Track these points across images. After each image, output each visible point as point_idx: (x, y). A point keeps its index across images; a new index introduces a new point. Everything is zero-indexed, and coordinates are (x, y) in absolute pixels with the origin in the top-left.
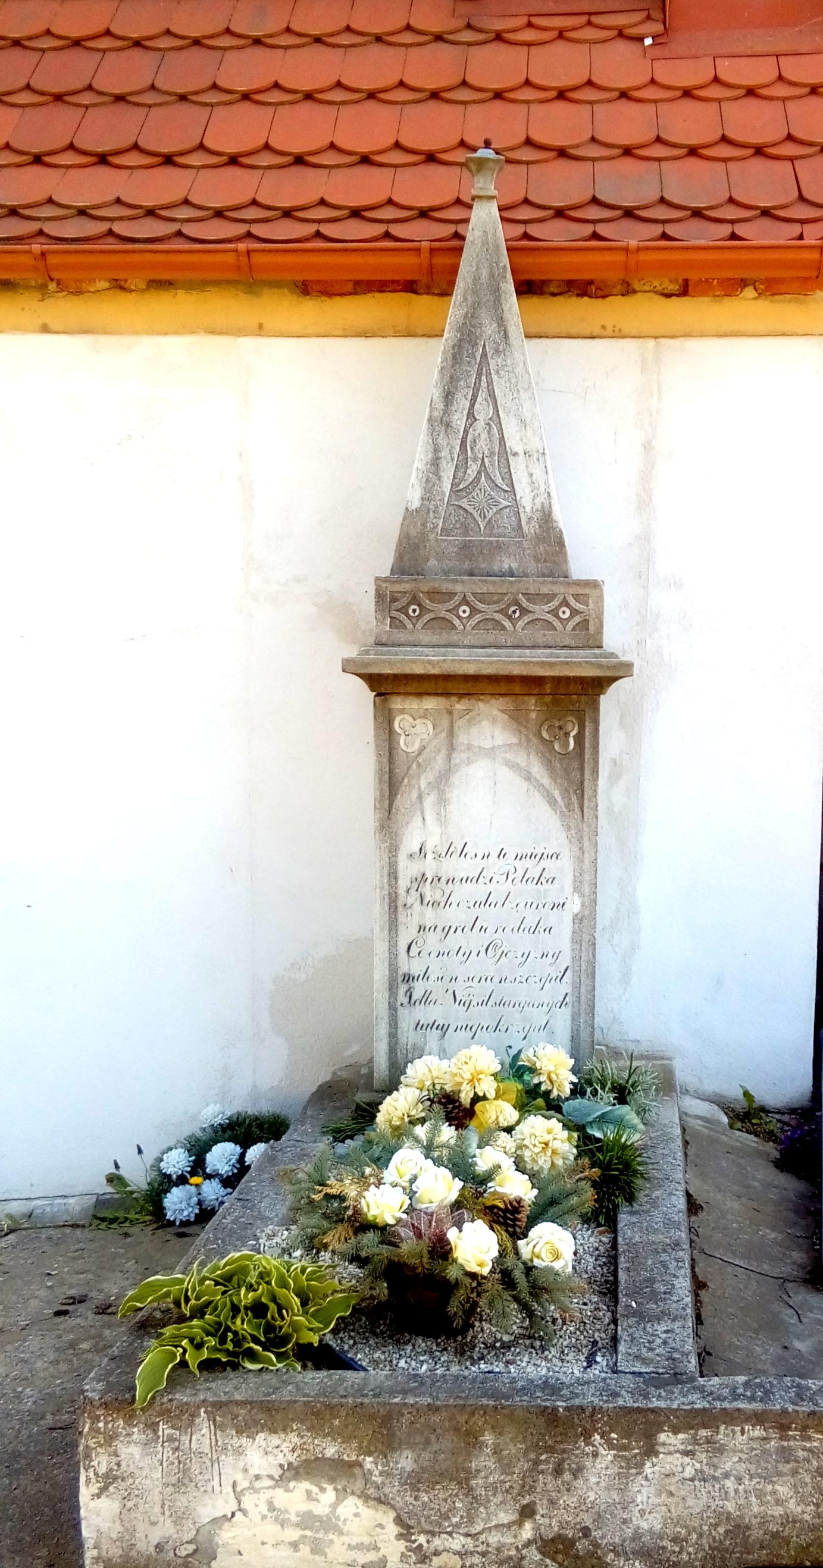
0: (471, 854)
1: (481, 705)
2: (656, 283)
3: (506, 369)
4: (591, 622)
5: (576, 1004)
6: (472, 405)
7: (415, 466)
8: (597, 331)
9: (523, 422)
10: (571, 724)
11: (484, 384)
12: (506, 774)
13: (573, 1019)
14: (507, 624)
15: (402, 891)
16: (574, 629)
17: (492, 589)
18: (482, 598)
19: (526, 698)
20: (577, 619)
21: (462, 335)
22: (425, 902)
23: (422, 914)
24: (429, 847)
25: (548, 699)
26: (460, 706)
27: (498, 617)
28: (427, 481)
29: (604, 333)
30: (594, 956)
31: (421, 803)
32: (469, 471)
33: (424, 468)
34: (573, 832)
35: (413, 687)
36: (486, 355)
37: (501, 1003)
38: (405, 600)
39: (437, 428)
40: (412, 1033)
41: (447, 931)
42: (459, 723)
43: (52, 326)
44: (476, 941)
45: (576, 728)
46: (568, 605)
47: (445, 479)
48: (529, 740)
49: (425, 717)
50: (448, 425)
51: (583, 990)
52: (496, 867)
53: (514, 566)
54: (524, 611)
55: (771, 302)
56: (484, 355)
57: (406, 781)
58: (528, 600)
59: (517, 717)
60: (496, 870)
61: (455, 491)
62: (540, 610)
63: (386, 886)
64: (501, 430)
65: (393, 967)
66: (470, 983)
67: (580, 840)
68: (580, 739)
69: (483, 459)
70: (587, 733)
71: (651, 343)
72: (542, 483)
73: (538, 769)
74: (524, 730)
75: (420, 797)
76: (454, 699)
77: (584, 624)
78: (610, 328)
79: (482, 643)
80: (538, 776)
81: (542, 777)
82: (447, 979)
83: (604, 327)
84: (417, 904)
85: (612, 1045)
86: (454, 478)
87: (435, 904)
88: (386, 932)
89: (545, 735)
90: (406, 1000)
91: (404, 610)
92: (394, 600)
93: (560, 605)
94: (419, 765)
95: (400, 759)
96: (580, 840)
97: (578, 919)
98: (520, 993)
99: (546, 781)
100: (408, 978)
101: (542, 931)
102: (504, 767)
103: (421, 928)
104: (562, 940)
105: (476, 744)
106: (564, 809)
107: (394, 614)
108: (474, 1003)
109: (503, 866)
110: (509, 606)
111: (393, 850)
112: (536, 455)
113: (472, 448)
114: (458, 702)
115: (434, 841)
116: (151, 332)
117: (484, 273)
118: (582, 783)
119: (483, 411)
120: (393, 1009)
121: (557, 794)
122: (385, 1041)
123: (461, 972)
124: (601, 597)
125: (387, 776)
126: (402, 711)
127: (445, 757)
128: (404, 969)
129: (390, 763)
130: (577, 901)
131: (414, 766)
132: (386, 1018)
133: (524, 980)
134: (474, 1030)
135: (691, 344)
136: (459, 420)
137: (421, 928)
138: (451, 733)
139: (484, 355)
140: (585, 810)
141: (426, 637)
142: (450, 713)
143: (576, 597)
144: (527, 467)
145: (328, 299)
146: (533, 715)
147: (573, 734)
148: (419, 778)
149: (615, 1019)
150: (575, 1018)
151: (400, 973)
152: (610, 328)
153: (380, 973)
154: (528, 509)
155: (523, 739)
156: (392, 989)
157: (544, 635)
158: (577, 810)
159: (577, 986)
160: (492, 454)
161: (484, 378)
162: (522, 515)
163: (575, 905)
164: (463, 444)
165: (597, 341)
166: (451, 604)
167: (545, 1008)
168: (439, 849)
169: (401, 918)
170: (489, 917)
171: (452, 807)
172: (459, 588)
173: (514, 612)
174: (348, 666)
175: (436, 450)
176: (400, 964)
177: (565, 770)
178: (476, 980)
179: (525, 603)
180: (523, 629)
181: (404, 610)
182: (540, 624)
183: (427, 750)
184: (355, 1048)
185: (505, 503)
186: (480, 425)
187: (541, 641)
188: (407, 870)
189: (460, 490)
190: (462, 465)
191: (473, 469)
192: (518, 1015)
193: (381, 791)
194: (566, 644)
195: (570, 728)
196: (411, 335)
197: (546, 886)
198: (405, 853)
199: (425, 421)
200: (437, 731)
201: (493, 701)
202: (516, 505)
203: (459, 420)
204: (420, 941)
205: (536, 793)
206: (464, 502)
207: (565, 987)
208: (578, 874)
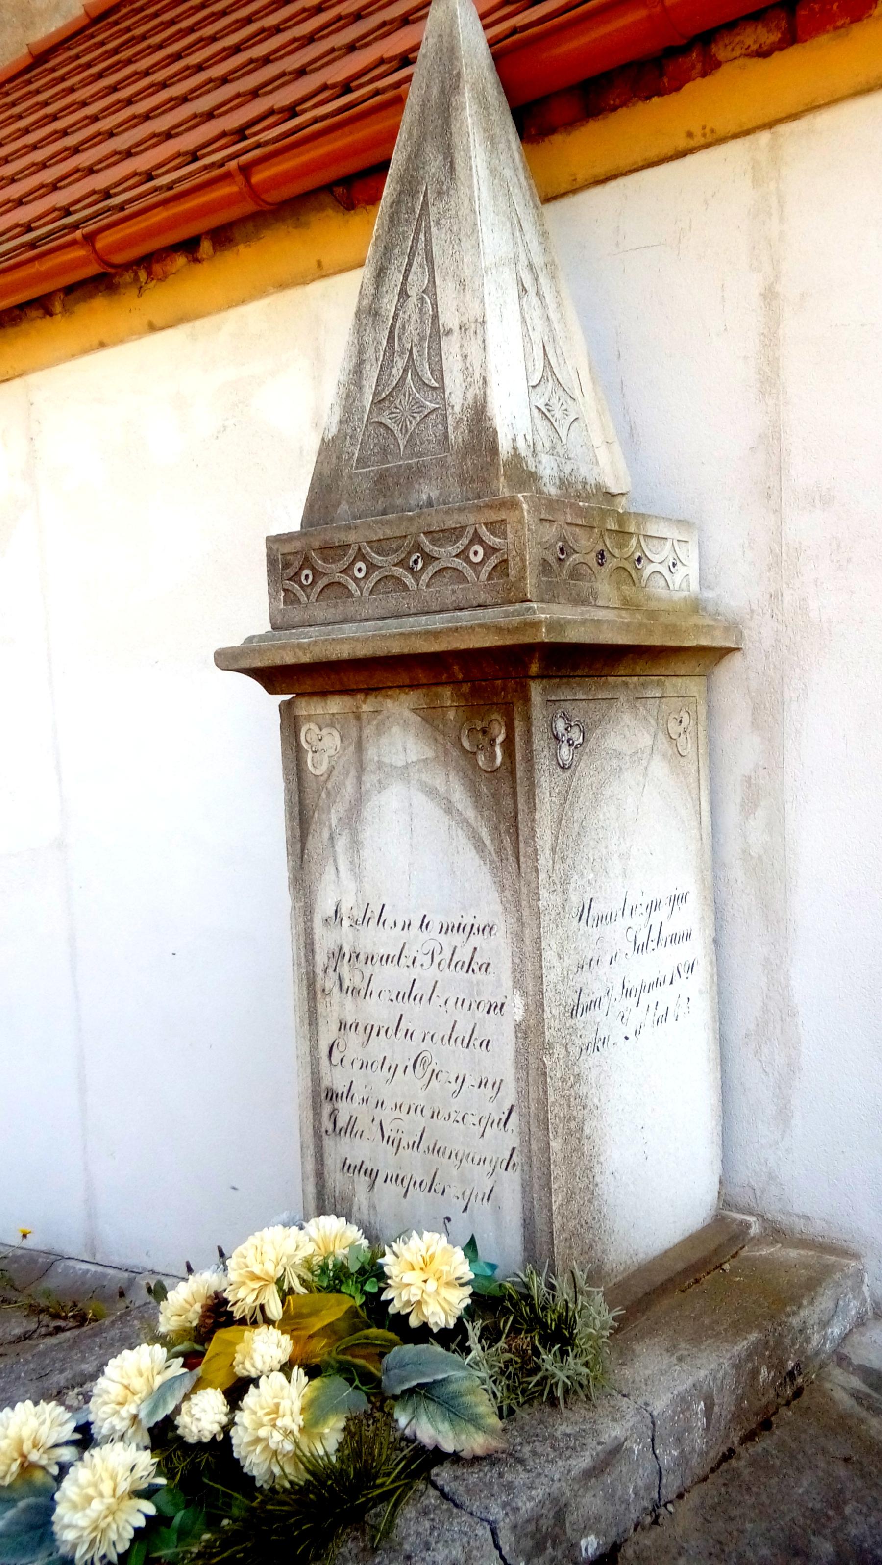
1: (389, 703)
2: (749, 41)
4: (511, 563)
5: (526, 1168)
6: (406, 277)
8: (682, 143)
9: (462, 284)
11: (421, 245)
12: (427, 810)
13: (524, 1192)
14: (409, 580)
15: (319, 970)
16: (490, 577)
17: (389, 533)
18: (380, 546)
19: (440, 689)
21: (403, 185)
22: (345, 987)
23: (342, 1005)
24: (344, 911)
28: (348, 396)
29: (692, 143)
31: (333, 847)
33: (346, 379)
36: (427, 204)
37: (435, 1150)
38: (297, 564)
41: (369, 1030)
42: (368, 731)
43: (158, 321)
44: (400, 1051)
45: (503, 731)
49: (332, 725)
50: (376, 314)
51: (534, 1147)
52: (420, 942)
53: (434, 494)
54: (429, 559)
56: (425, 203)
57: (316, 815)
58: (433, 542)
59: (430, 717)
60: (419, 947)
61: (378, 403)
62: (446, 554)
63: (303, 964)
64: (435, 306)
67: (518, 904)
68: (509, 745)
69: (411, 351)
70: (517, 739)
71: (764, 137)
72: (477, 365)
73: (459, 796)
74: (440, 738)
75: (331, 838)
76: (361, 696)
78: (698, 132)
81: (466, 808)
82: (372, 1102)
83: (690, 135)
84: (336, 989)
85: (769, 1216)
86: (377, 385)
87: (355, 991)
88: (307, 1027)
89: (466, 744)
90: (330, 1127)
91: (295, 577)
92: (286, 565)
94: (329, 794)
95: (311, 785)
96: (518, 904)
98: (455, 1136)
99: (470, 813)
100: (332, 1095)
101: (477, 1043)
102: (420, 793)
104: (502, 1062)
105: (386, 760)
108: (404, 1144)
109: (432, 938)
110: (410, 554)
113: (399, 337)
114: (364, 702)
116: (232, 304)
117: (435, 91)
119: (417, 281)
121: (484, 833)
126: (309, 718)
127: (355, 781)
128: (326, 1083)
129: (300, 791)
130: (519, 1002)
131: (324, 795)
135: (823, 119)
136: (389, 304)
137: (342, 1026)
140: (522, 859)
141: (321, 612)
142: (358, 718)
143: (491, 526)
144: (462, 346)
146: (451, 714)
147: (499, 740)
148: (329, 812)
149: (771, 1177)
150: (526, 1188)
151: (323, 1086)
152: (698, 132)
154: (457, 409)
155: (441, 752)
157: (454, 592)
159: (526, 1138)
160: (422, 339)
161: (422, 236)
163: (517, 1009)
165: (690, 159)
166: (344, 563)
167: (488, 1168)
168: (355, 912)
169: (321, 1008)
170: (417, 1015)
171: (366, 852)
172: (352, 537)
173: (416, 562)
174: (227, 660)
175: (361, 352)
176: (323, 1073)
177: (494, 795)
179: (428, 547)
180: (428, 586)
181: (295, 577)
182: (448, 574)
183: (335, 773)
185: (433, 406)
186: (413, 301)
187: (450, 600)
189: (383, 400)
190: (386, 367)
192: (455, 1172)
194: (481, 602)
195: (496, 731)
197: (480, 976)
200: (347, 743)
201: (403, 697)
202: (445, 404)
205: (460, 832)
208: (517, 961)
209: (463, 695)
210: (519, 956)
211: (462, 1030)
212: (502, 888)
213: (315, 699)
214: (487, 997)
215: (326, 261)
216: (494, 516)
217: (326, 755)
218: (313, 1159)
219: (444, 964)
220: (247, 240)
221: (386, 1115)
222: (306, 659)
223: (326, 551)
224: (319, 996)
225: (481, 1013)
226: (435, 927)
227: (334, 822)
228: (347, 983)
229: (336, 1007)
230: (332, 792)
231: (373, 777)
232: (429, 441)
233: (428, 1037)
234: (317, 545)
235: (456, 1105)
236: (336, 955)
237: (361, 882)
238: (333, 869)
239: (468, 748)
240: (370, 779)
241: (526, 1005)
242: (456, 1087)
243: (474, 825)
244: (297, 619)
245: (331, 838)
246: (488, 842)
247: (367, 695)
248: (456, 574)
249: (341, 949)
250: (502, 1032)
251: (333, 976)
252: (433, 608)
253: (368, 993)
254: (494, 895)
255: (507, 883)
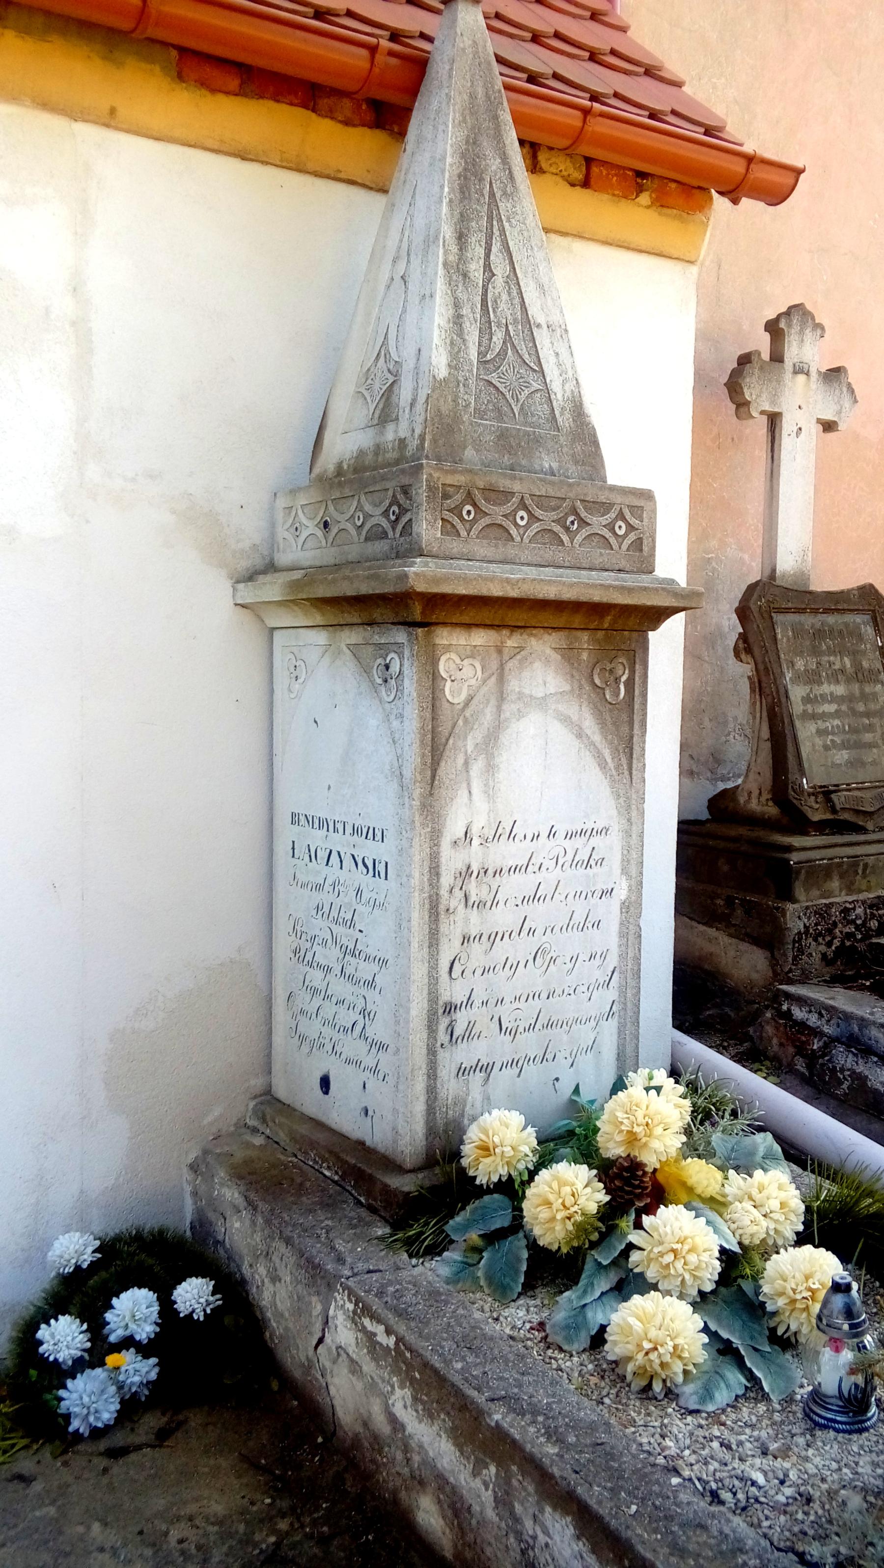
0: (520, 836)
1: (533, 641)
3: (517, 218)
4: (645, 542)
7: (436, 324)
9: (541, 287)
10: (621, 667)
12: (560, 734)
13: (619, 1033)
15: (444, 892)
16: (628, 550)
19: (579, 633)
20: (632, 537)
21: (466, 162)
22: (470, 903)
23: (467, 920)
24: (475, 831)
25: (600, 634)
26: (512, 641)
27: (557, 528)
28: (452, 343)
30: (640, 950)
32: (495, 339)
34: (621, 800)
35: (486, 615)
36: (494, 195)
37: (549, 1025)
39: (454, 278)
40: (453, 1081)
41: (492, 938)
45: (627, 672)
46: (624, 519)
47: (471, 345)
48: (581, 687)
49: (472, 656)
50: (465, 275)
51: (629, 995)
53: (555, 465)
54: (583, 523)
55: (660, 214)
57: (451, 741)
59: (568, 654)
61: (482, 363)
62: (598, 522)
63: (427, 888)
65: (433, 996)
66: (517, 1005)
70: (637, 679)
72: (569, 366)
73: (590, 724)
75: (466, 763)
76: (505, 632)
77: (638, 544)
79: (538, 560)
80: (589, 732)
81: (594, 733)
82: (492, 1002)
87: (481, 905)
88: (426, 950)
89: (597, 681)
91: (457, 511)
92: (446, 496)
93: (616, 519)
94: (466, 721)
95: (446, 712)
97: (626, 907)
98: (565, 1008)
99: (597, 738)
100: (450, 1008)
101: (590, 926)
102: (556, 722)
103: (466, 939)
104: (608, 938)
105: (527, 691)
106: (614, 772)
107: (447, 515)
108: (521, 1029)
111: (435, 837)
112: (559, 330)
113: (494, 311)
115: (480, 822)
117: (480, 92)
118: (632, 737)
120: (432, 1052)
121: (607, 754)
122: (423, 1099)
123: (507, 990)
124: (654, 511)
125: (430, 736)
126: (448, 648)
127: (494, 710)
128: (445, 997)
131: (460, 722)
132: (424, 1066)
133: (572, 992)
134: (520, 1064)
135: (578, 246)
136: (476, 270)
137: (466, 939)
138: (501, 679)
139: (492, 195)
140: (634, 772)
141: (482, 549)
142: (499, 650)
145: (207, 93)
146: (585, 656)
148: (465, 738)
151: (441, 1003)
153: (418, 1008)
154: (559, 396)
155: (576, 686)
156: (431, 1027)
158: (626, 773)
159: (622, 991)
160: (515, 321)
161: (495, 223)
162: (555, 403)
163: (622, 892)
164: (484, 302)
166: (508, 508)
167: (593, 1023)
169: (443, 928)
171: (501, 776)
172: (517, 487)
173: (572, 523)
175: (457, 305)
177: (614, 723)
178: (523, 998)
179: (583, 514)
182: (596, 539)
183: (474, 702)
184: (217, 1112)
187: (598, 561)
188: (452, 861)
190: (486, 330)
191: (498, 337)
192: (565, 1038)
193: (423, 755)
194: (621, 567)
196: (300, 169)
197: (596, 870)
198: (448, 839)
199: (440, 266)
201: (546, 637)
202: (547, 390)
203: (476, 270)
204: (464, 956)
205: (588, 753)
206: (494, 378)
207: (612, 994)
208: (625, 852)
209: (598, 641)
210: (627, 849)
211: (579, 918)
212: (618, 796)
213: (458, 630)
214: (600, 886)
215: (122, 112)
216: (636, 502)
217: (467, 684)
218: (425, 1077)
219: (567, 865)
220: (25, 31)
221: (506, 1012)
222: (514, 593)
223: (487, 492)
224: (442, 916)
225: (595, 900)
226: (561, 835)
227: (470, 748)
228: (473, 898)
229: (460, 922)
230: (470, 719)
231: (513, 706)
232: (540, 417)
233: (549, 930)
234: (481, 485)
235: (571, 980)
236: (463, 874)
237: (494, 802)
238: (466, 792)
239: (599, 684)
240: (509, 708)
241: (630, 886)
242: (570, 966)
243: (600, 747)
244: (455, 550)
245: (466, 763)
246: (609, 760)
247: (512, 631)
248: (602, 540)
249: (469, 867)
250: (610, 913)
251: (458, 894)
252: (584, 565)
253: (494, 903)
254: (612, 803)
255: (622, 792)
